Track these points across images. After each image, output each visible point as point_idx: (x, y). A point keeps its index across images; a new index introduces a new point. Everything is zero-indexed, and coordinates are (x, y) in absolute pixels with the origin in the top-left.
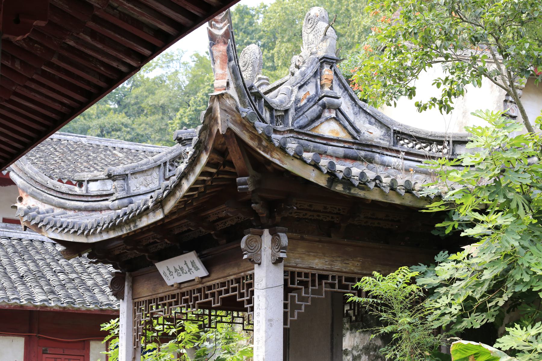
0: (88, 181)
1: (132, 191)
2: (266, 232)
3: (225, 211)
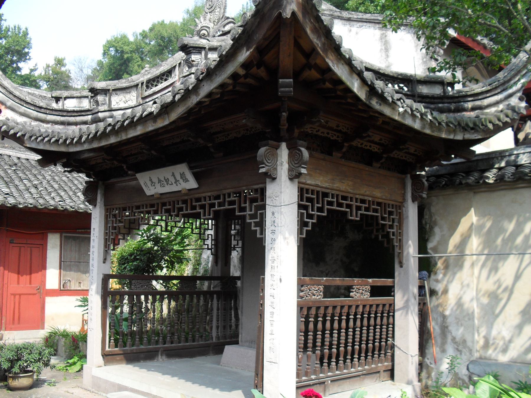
0: (66, 98)
1: (112, 106)
2: (284, 145)
3: (245, 122)
